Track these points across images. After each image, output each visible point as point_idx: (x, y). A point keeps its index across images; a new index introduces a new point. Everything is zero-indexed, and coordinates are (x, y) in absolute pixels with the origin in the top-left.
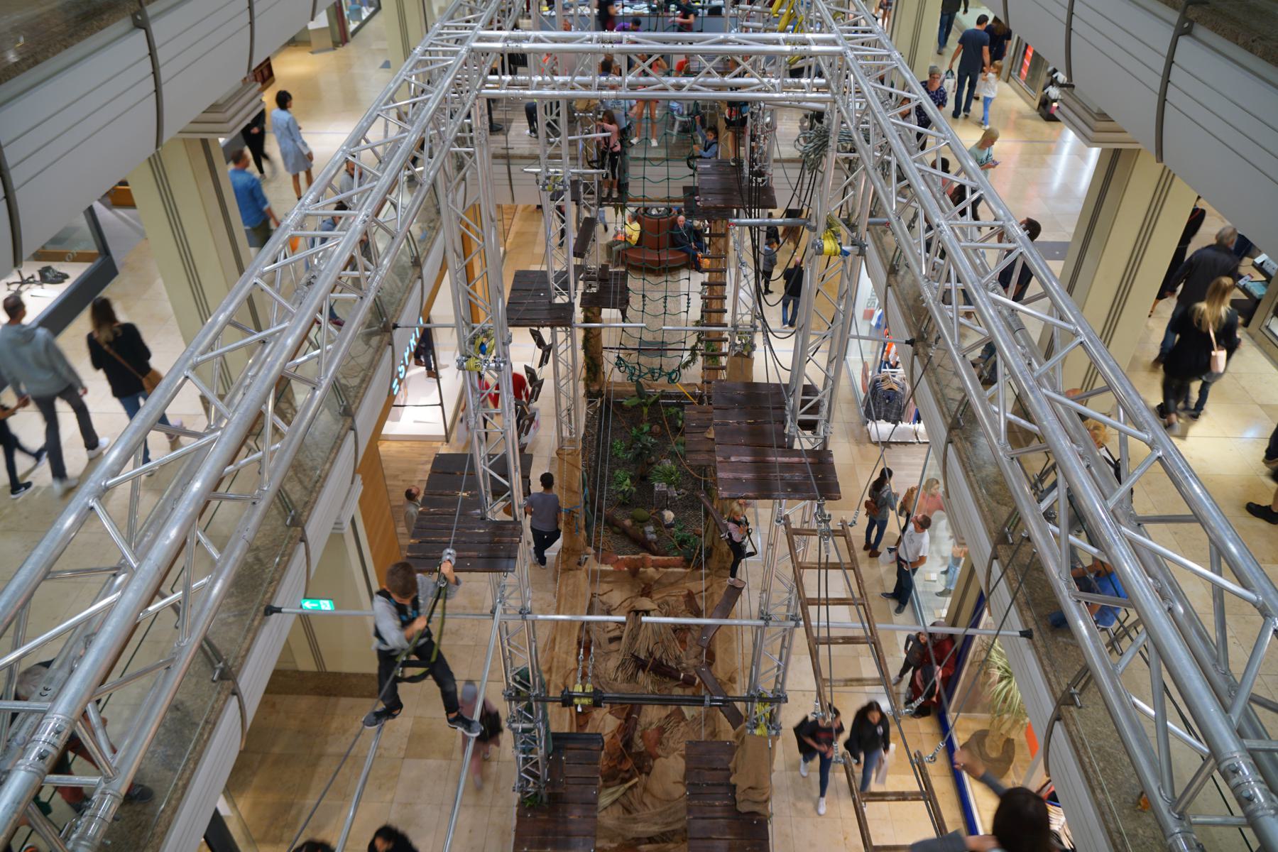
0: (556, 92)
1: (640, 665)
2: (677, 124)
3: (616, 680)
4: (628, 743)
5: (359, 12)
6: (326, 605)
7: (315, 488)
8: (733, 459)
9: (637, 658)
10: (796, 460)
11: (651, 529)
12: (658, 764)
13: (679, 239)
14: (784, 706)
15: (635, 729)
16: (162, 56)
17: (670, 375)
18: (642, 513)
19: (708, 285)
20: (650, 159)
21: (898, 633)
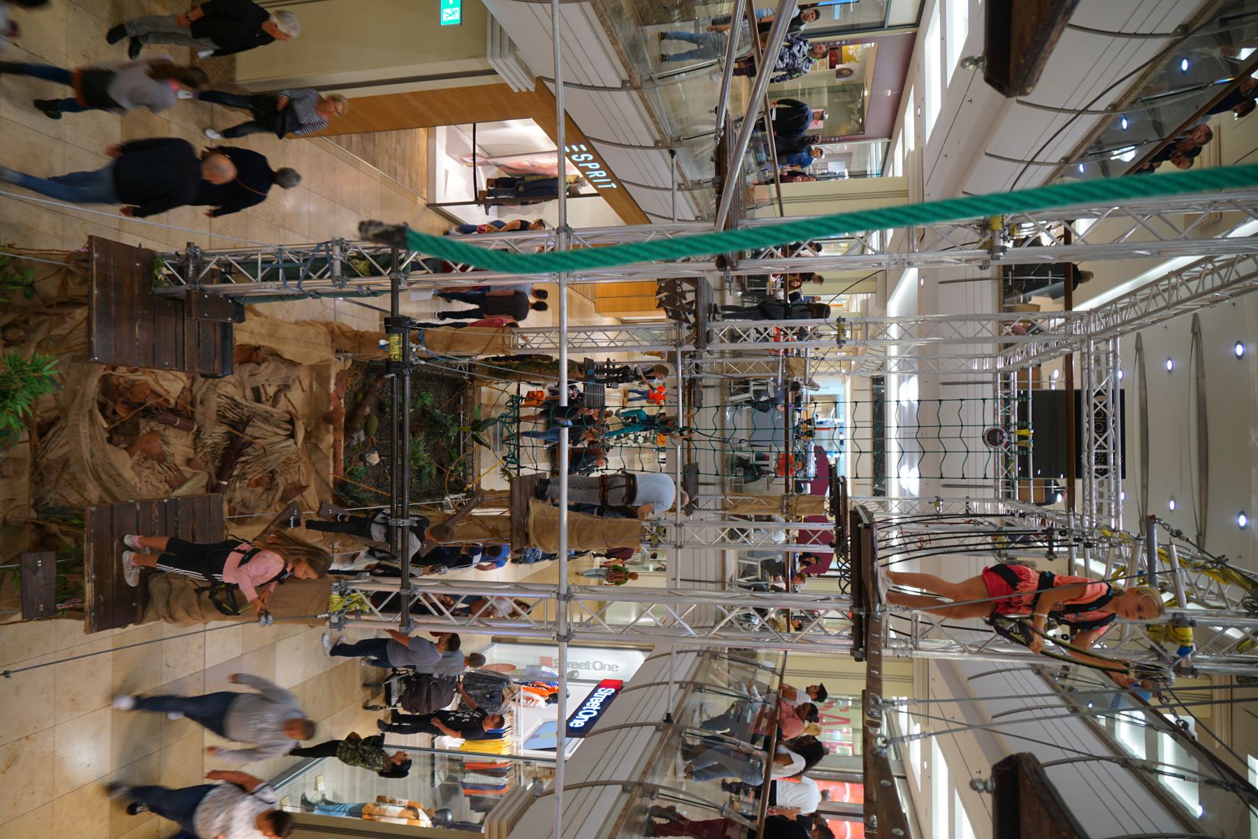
4: (148, 413)
16: (604, 93)
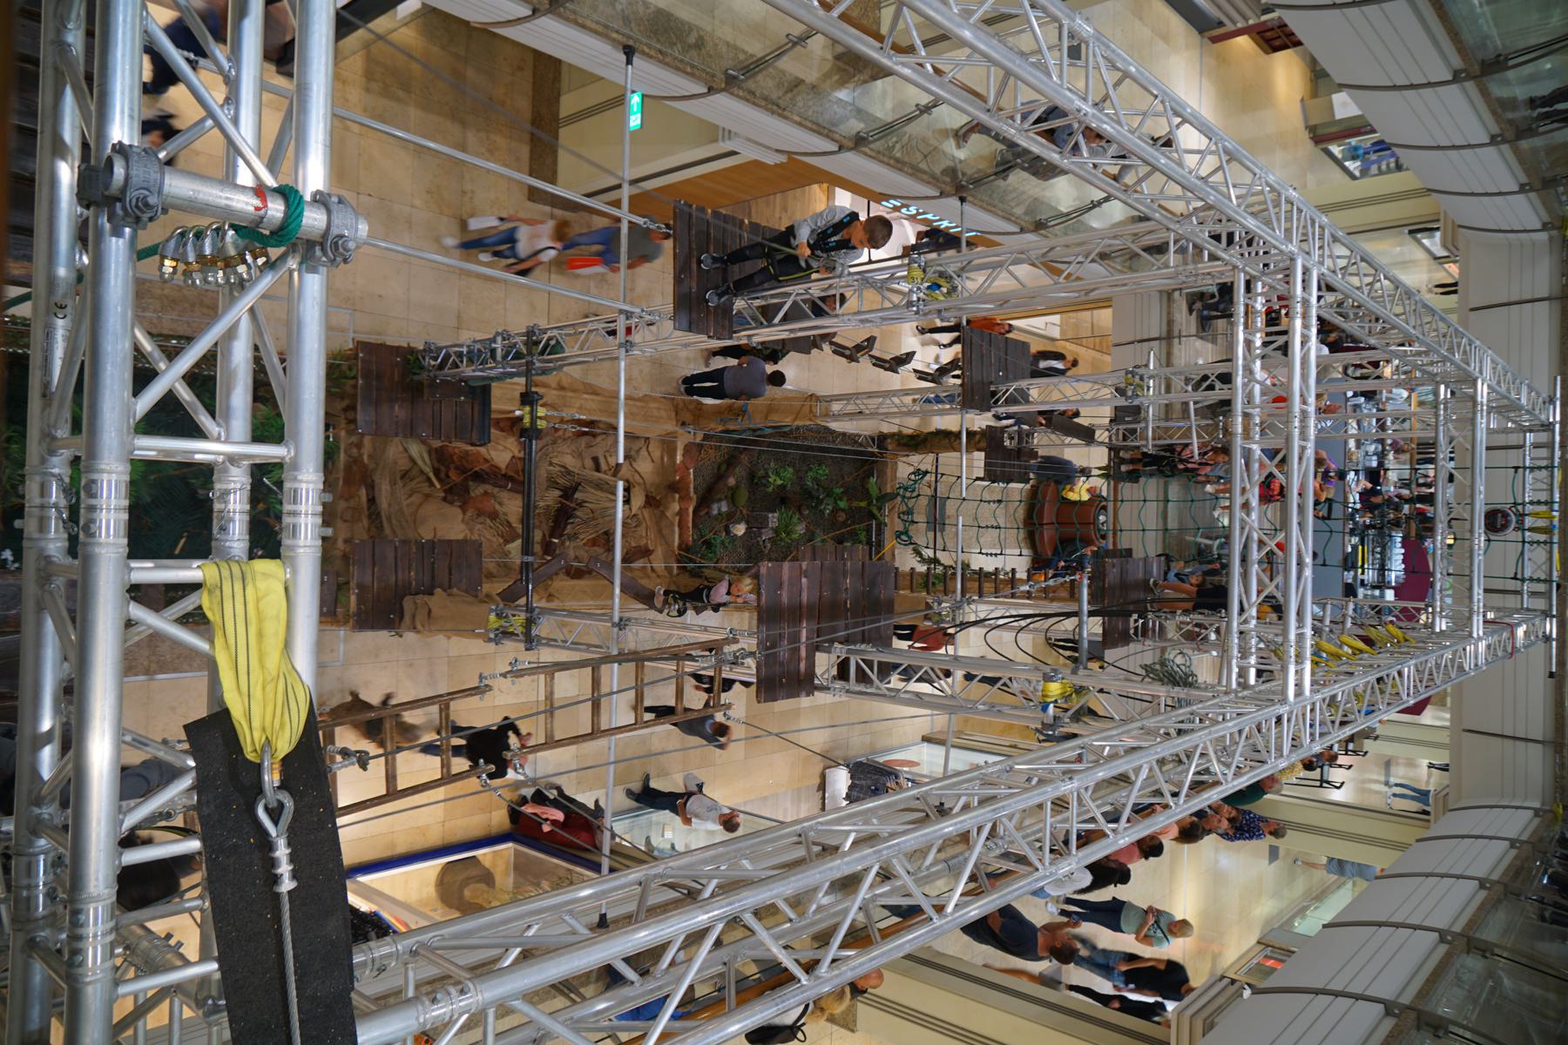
0: (1240, 362)
1: (568, 493)
2: (1208, 542)
3: (551, 464)
4: (479, 477)
5: (1354, 158)
6: (635, 121)
7: (776, 108)
8: (804, 580)
9: (575, 489)
10: (803, 653)
11: (724, 509)
12: (455, 511)
13: (1069, 549)
14: (522, 646)
15: (495, 485)
16: (1427, 93)
17: (906, 533)
18: (743, 496)
19: (1013, 581)
20: (1166, 508)
21: (603, 791)
